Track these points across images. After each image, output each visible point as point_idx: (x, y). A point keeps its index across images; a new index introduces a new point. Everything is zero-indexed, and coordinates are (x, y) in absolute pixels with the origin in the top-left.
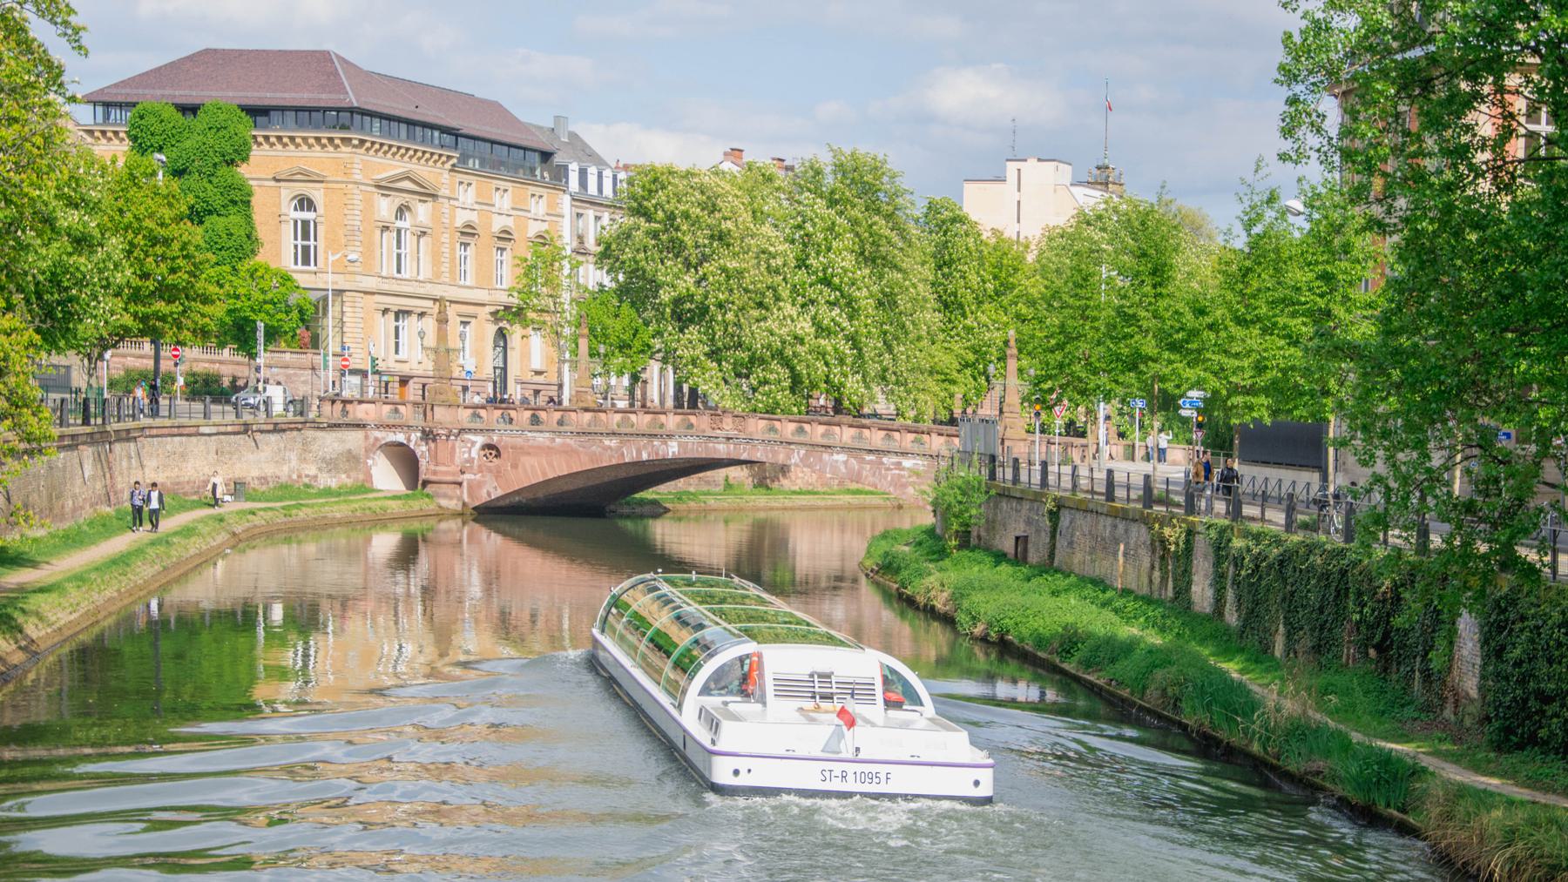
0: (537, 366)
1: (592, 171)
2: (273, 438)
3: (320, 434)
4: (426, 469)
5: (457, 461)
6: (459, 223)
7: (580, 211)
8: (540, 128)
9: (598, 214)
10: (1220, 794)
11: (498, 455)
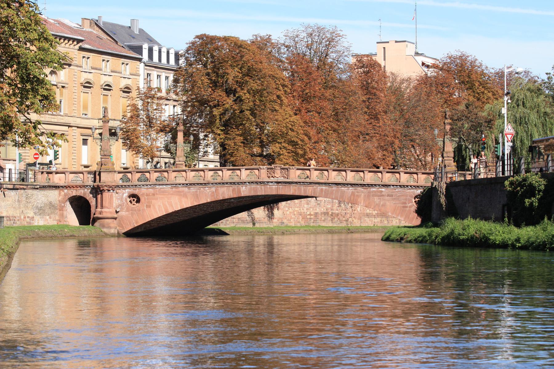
0: (85, 162)
1: (156, 49)
2: (13, 193)
3: (35, 192)
4: (95, 211)
5: (114, 205)
6: (82, 80)
7: (149, 72)
8: (123, 27)
9: (159, 74)
10: (275, 295)
11: (138, 201)
